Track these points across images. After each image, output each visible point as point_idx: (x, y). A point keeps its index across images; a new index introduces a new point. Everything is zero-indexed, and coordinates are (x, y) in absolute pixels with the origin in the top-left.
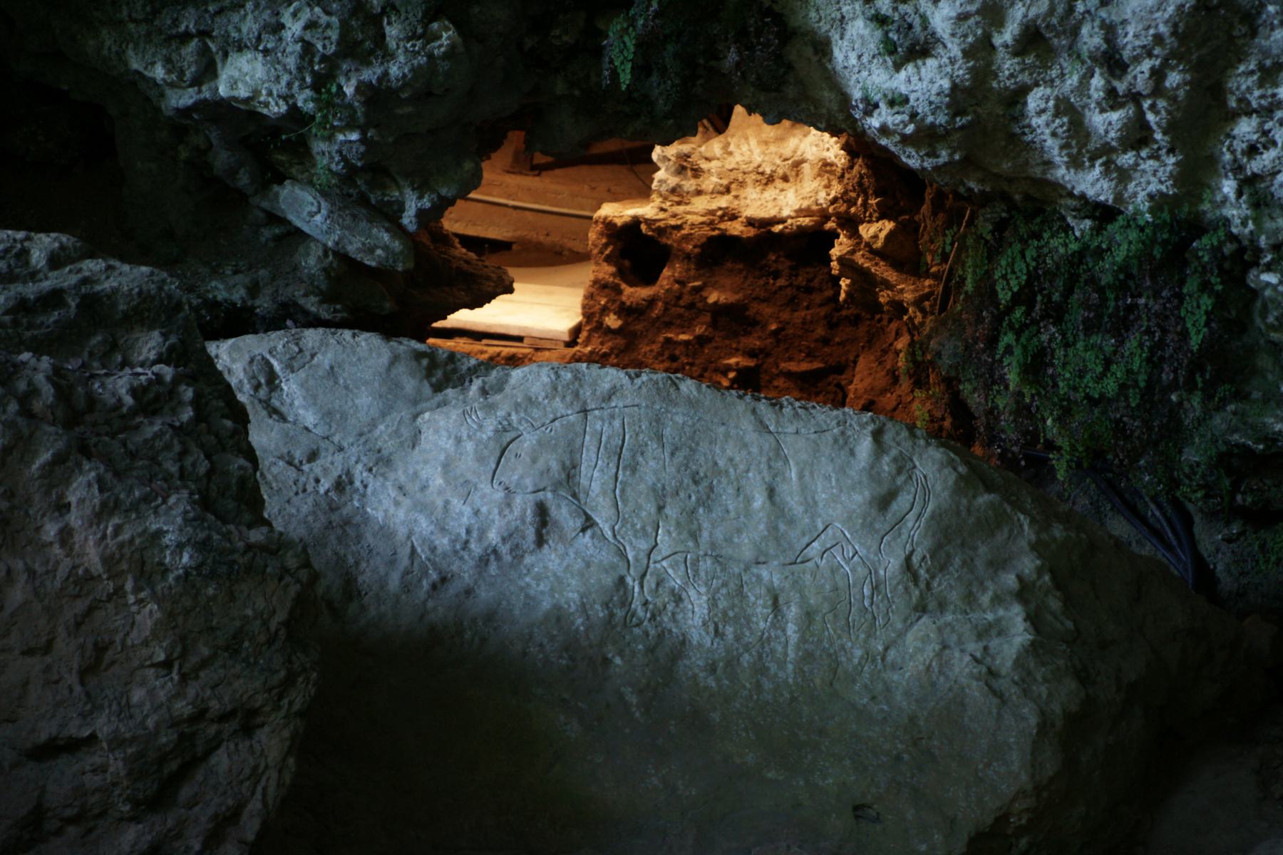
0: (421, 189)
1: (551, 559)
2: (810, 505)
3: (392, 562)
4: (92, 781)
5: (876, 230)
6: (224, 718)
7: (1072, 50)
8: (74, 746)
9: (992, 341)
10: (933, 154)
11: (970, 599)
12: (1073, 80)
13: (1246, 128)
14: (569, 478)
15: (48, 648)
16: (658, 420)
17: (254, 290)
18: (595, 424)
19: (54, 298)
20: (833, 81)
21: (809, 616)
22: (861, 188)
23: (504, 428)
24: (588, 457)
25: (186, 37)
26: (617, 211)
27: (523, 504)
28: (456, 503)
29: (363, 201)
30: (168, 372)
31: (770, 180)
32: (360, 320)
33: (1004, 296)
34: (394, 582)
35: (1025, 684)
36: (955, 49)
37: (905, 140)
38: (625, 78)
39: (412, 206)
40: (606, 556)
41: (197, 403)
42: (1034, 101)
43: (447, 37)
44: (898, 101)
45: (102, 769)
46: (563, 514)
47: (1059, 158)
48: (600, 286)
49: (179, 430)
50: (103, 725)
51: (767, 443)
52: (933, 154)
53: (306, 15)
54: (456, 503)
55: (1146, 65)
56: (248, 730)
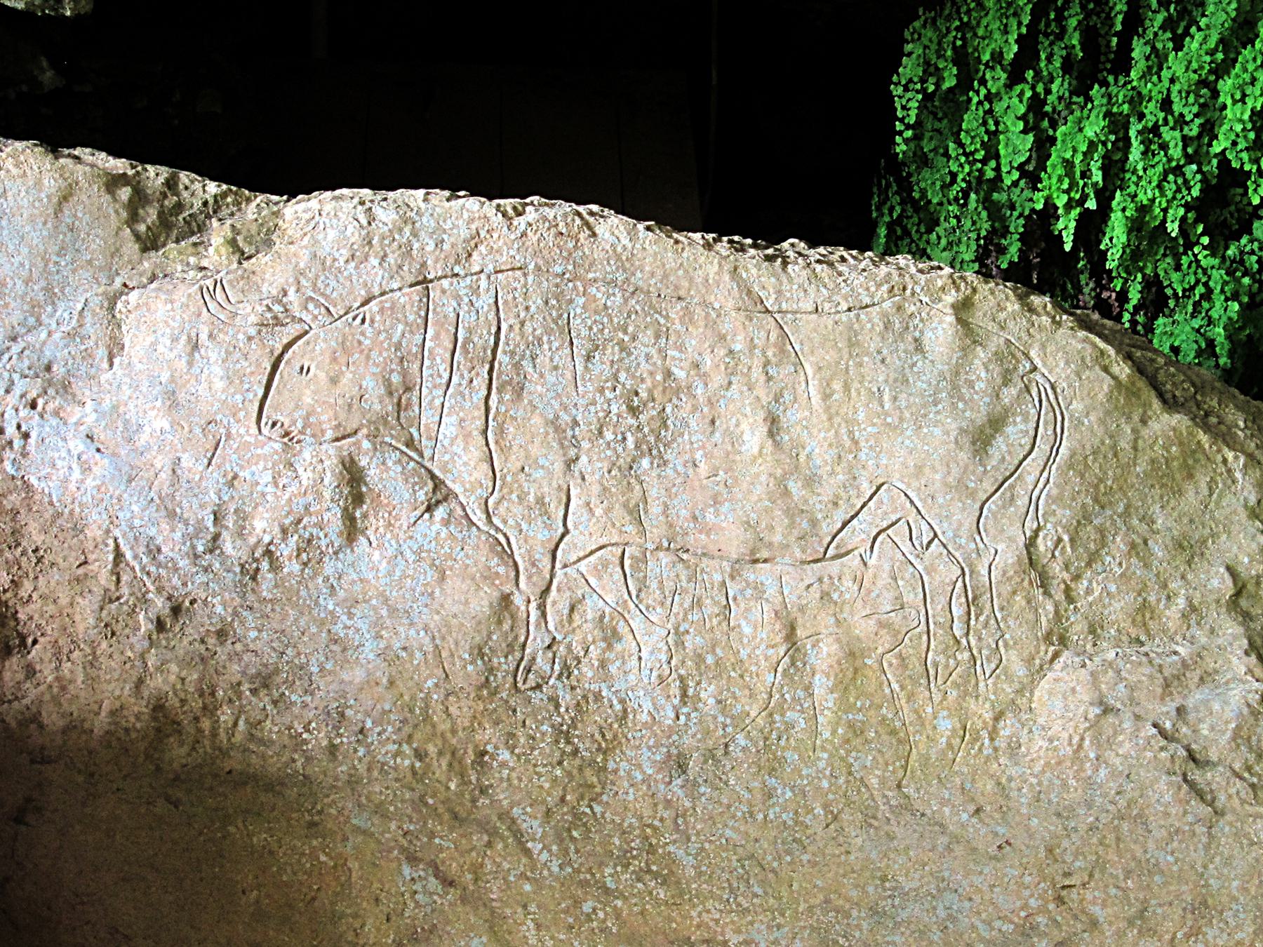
34: (86, 616)
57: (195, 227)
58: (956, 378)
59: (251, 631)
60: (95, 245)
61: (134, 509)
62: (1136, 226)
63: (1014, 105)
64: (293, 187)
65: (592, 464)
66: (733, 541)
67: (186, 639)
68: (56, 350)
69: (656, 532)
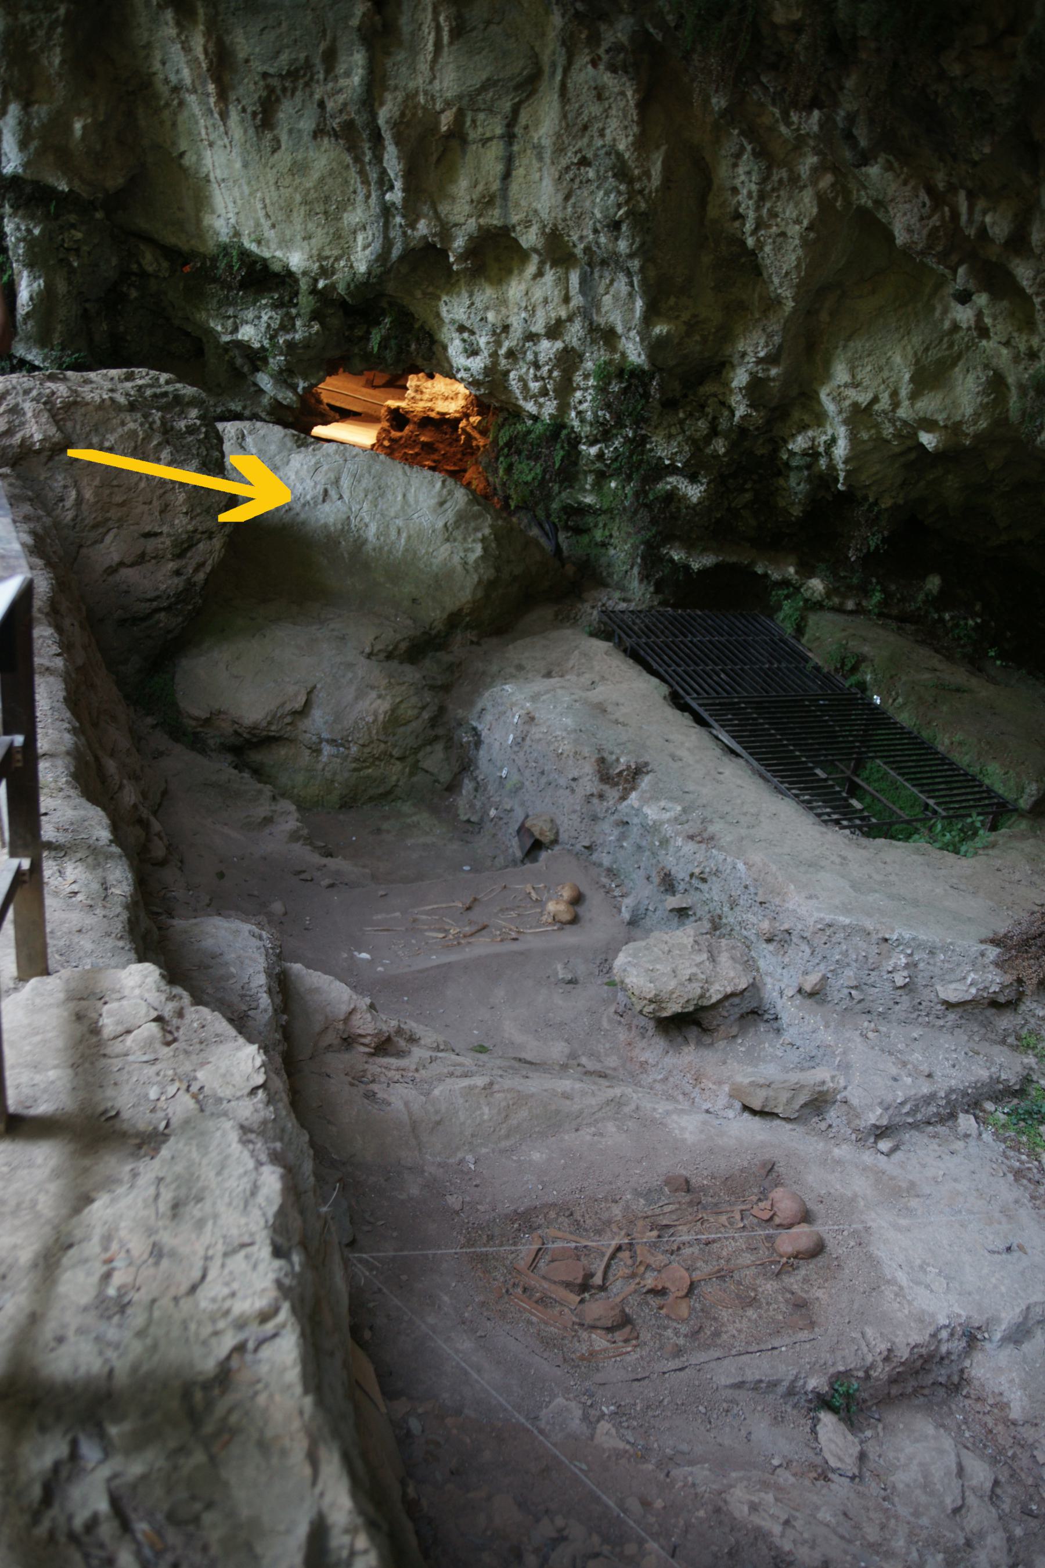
0: (305, 379)
1: (327, 507)
2: (417, 502)
4: (160, 546)
5: (475, 419)
6: (203, 533)
7: (523, 359)
8: (156, 535)
9: (497, 459)
11: (465, 539)
12: (524, 370)
13: (578, 394)
14: (337, 481)
15: (150, 503)
16: (370, 467)
17: (244, 408)
18: (349, 465)
19: (165, 394)
20: (448, 360)
21: (409, 537)
22: (472, 403)
23: (317, 463)
24: (344, 476)
25: (229, 317)
26: (393, 403)
27: (320, 488)
28: (298, 485)
29: (285, 382)
30: (198, 422)
31: (447, 398)
32: (279, 422)
33: (501, 443)
35: (476, 569)
36: (486, 353)
38: (376, 349)
39: (302, 385)
40: (345, 509)
41: (206, 433)
42: (512, 375)
43: (316, 327)
44: (467, 369)
45: (163, 543)
46: (333, 493)
47: (520, 397)
48: (384, 430)
49: (199, 441)
50: (165, 529)
51: (406, 479)
54: (298, 485)
55: (547, 368)
56: (210, 538)
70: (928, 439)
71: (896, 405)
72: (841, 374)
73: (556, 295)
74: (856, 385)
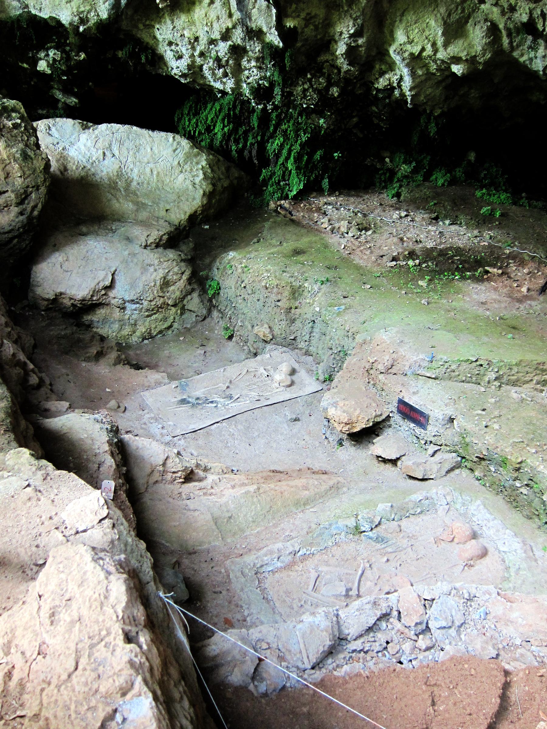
3: (74, 164)
4: (9, 199)
6: (33, 187)
10: (186, 79)
34: (74, 168)
37: (180, 76)
41: (25, 126)
46: (108, 153)
49: (22, 132)
52: (186, 79)
53: (53, 52)
57: (89, 128)
58: (172, 145)
59: (92, 170)
60: (77, 129)
61: (80, 157)
62: (199, 132)
63: (187, 119)
64: (100, 124)
65: (131, 153)
66: (146, 160)
67: (85, 170)
68: (72, 140)
69: (137, 160)
70: (457, 69)
71: (436, 51)
72: (400, 37)
73: (224, 14)
74: (411, 42)
